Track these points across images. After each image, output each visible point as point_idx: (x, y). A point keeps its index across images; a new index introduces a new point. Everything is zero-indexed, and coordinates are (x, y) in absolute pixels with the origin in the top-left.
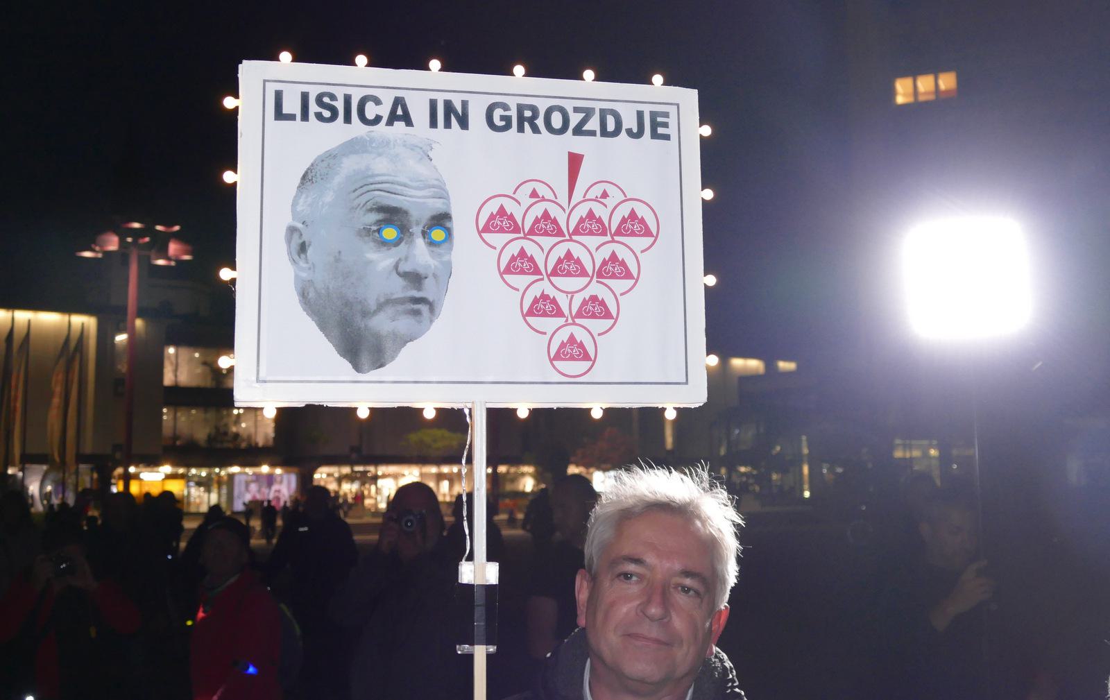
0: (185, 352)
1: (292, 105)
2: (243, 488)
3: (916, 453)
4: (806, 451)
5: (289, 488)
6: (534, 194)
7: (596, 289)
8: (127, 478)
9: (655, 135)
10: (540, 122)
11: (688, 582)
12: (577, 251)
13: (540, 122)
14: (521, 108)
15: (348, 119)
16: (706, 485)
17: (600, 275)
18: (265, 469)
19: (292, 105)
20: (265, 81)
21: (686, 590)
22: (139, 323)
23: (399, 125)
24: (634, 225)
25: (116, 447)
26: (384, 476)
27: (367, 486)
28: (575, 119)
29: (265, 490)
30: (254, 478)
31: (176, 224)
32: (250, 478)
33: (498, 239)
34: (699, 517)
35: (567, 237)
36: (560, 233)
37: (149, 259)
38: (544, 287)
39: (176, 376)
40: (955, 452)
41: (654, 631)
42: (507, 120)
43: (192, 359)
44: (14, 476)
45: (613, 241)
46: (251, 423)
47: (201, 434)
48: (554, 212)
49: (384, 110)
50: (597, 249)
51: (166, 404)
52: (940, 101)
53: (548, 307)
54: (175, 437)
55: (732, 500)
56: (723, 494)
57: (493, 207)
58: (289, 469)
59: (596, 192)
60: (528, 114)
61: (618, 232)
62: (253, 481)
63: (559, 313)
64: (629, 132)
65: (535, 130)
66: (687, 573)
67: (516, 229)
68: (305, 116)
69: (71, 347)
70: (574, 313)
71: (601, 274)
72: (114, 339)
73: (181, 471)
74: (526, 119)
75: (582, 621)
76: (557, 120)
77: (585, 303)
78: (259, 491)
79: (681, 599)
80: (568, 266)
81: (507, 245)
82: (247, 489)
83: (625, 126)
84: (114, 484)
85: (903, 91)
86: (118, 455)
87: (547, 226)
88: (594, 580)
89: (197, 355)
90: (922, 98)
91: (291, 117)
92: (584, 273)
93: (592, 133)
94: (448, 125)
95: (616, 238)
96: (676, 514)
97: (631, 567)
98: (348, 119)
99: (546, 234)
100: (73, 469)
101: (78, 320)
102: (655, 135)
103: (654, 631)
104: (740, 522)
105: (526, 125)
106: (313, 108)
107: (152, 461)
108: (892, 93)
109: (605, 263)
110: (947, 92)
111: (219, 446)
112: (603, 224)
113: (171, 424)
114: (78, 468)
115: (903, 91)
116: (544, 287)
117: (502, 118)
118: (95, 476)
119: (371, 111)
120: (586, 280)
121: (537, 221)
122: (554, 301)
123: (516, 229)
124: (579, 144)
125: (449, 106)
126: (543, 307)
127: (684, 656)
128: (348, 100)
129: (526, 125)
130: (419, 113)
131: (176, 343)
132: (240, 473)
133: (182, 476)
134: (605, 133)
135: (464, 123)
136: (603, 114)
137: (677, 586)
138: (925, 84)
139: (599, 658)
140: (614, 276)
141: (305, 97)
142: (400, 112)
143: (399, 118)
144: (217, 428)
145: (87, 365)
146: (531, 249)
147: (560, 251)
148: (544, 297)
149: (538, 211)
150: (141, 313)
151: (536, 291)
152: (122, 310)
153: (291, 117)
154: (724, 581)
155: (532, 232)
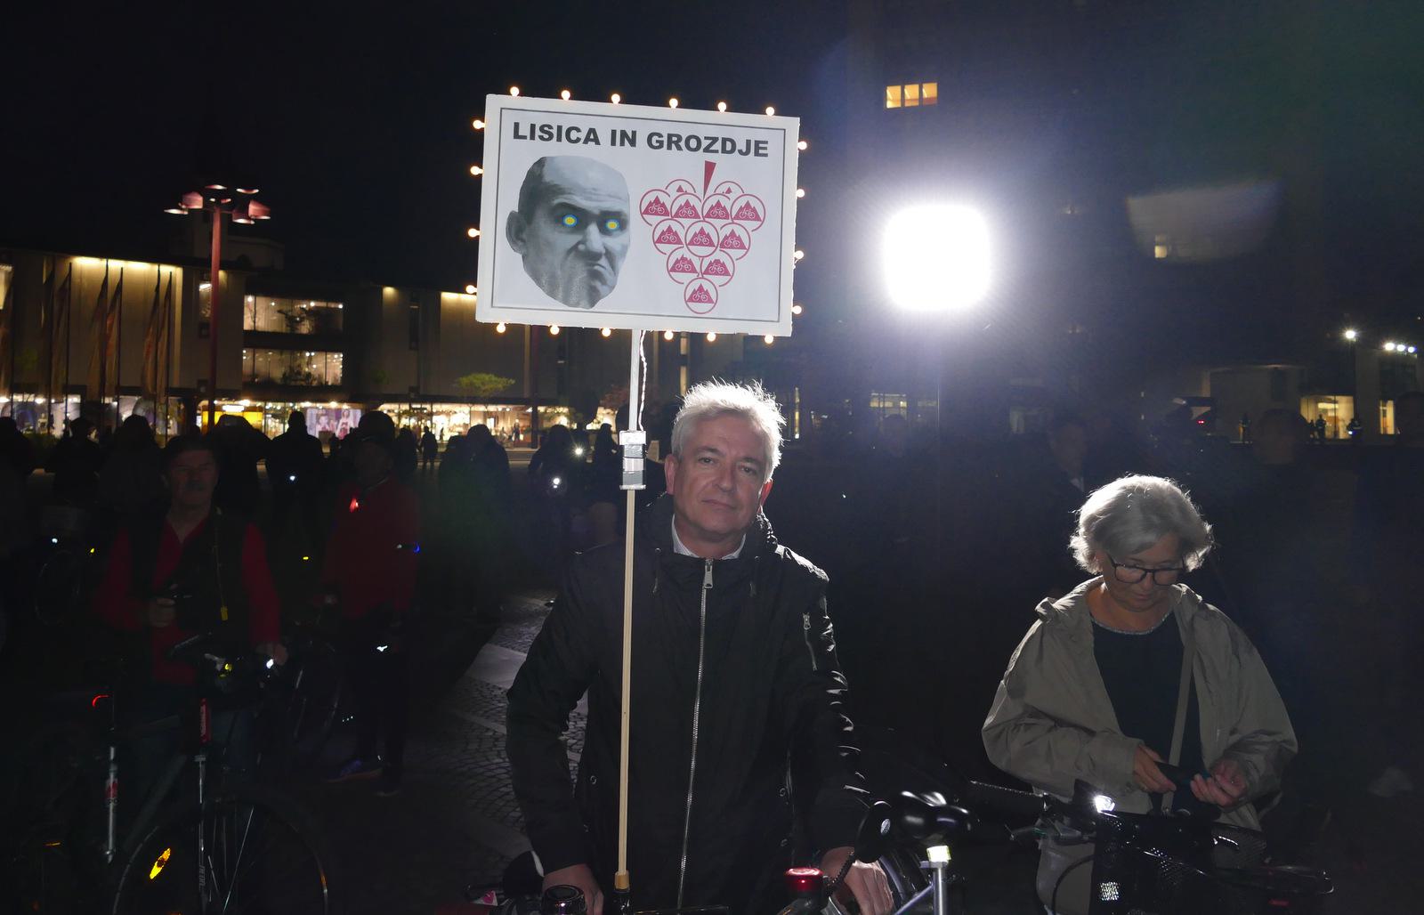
0: (262, 301)
1: (524, 130)
2: (314, 421)
3: (889, 404)
4: (798, 400)
5: (354, 422)
6: (680, 189)
7: (719, 255)
8: (212, 409)
9: (757, 154)
10: (682, 144)
11: (748, 465)
12: (708, 229)
13: (682, 144)
14: (670, 136)
15: (559, 139)
16: (761, 397)
17: (722, 246)
18: (333, 405)
19: (524, 130)
20: (502, 109)
21: (748, 470)
22: (221, 274)
23: (592, 144)
24: (749, 213)
25: (201, 382)
26: (438, 413)
27: (423, 421)
28: (705, 143)
29: (334, 423)
30: (324, 412)
31: (256, 189)
32: (320, 412)
33: (654, 219)
34: (756, 420)
35: (702, 219)
36: (697, 216)
37: (230, 217)
38: (683, 252)
39: (255, 322)
40: (920, 404)
41: (725, 499)
42: (661, 143)
43: (268, 307)
44: (109, 405)
45: (733, 223)
46: (321, 365)
47: (277, 373)
48: (693, 201)
49: (583, 135)
50: (721, 228)
51: (246, 347)
52: (923, 107)
53: (686, 266)
54: (254, 375)
55: (778, 407)
56: (772, 403)
57: (651, 198)
58: (354, 404)
59: (723, 189)
60: (674, 139)
61: (737, 217)
62: (322, 415)
63: (694, 271)
64: (740, 152)
65: (679, 148)
66: (748, 459)
67: (666, 213)
68: (532, 137)
69: (160, 294)
70: (703, 270)
71: (724, 245)
72: (198, 288)
73: (259, 404)
74: (673, 141)
75: (670, 490)
76: (693, 143)
77: (711, 264)
78: (328, 423)
79: (742, 475)
80: (702, 239)
81: (660, 224)
82: (318, 422)
83: (738, 148)
84: (199, 415)
85: (892, 98)
86: (202, 390)
87: (687, 211)
88: (680, 463)
89: (273, 304)
90: (907, 104)
91: (525, 137)
92: (711, 244)
93: (717, 151)
94: (622, 144)
95: (735, 221)
96: (740, 417)
97: (708, 455)
98: (559, 139)
99: (687, 217)
100: (163, 400)
101: (166, 270)
102: (757, 154)
103: (725, 499)
104: (784, 423)
105: (673, 145)
106: (538, 133)
107: (234, 396)
108: (883, 98)
109: (726, 237)
110: (929, 99)
111: (293, 383)
112: (665, 208)
113: (251, 363)
114: (167, 400)
115: (892, 98)
116: (683, 252)
117: (657, 141)
118: (182, 407)
119: (574, 135)
120: (712, 249)
121: (681, 207)
122: (690, 262)
123: (666, 213)
124: (710, 157)
125: (624, 134)
126: (682, 266)
127: (742, 516)
128: (560, 128)
129: (673, 145)
130: (605, 137)
131: (255, 294)
132: (311, 408)
133: (261, 409)
134: (724, 151)
135: (633, 143)
136: (724, 140)
137: (740, 467)
138: (911, 92)
139: (683, 515)
140: (732, 247)
141: (533, 126)
142: (592, 137)
143: (592, 140)
144: (291, 368)
145: (174, 308)
146: (676, 227)
147: (696, 228)
148: (683, 259)
149: (682, 201)
150: (222, 267)
151: (677, 255)
152: (207, 262)
153: (525, 137)
154: (771, 464)
155: (677, 215)
